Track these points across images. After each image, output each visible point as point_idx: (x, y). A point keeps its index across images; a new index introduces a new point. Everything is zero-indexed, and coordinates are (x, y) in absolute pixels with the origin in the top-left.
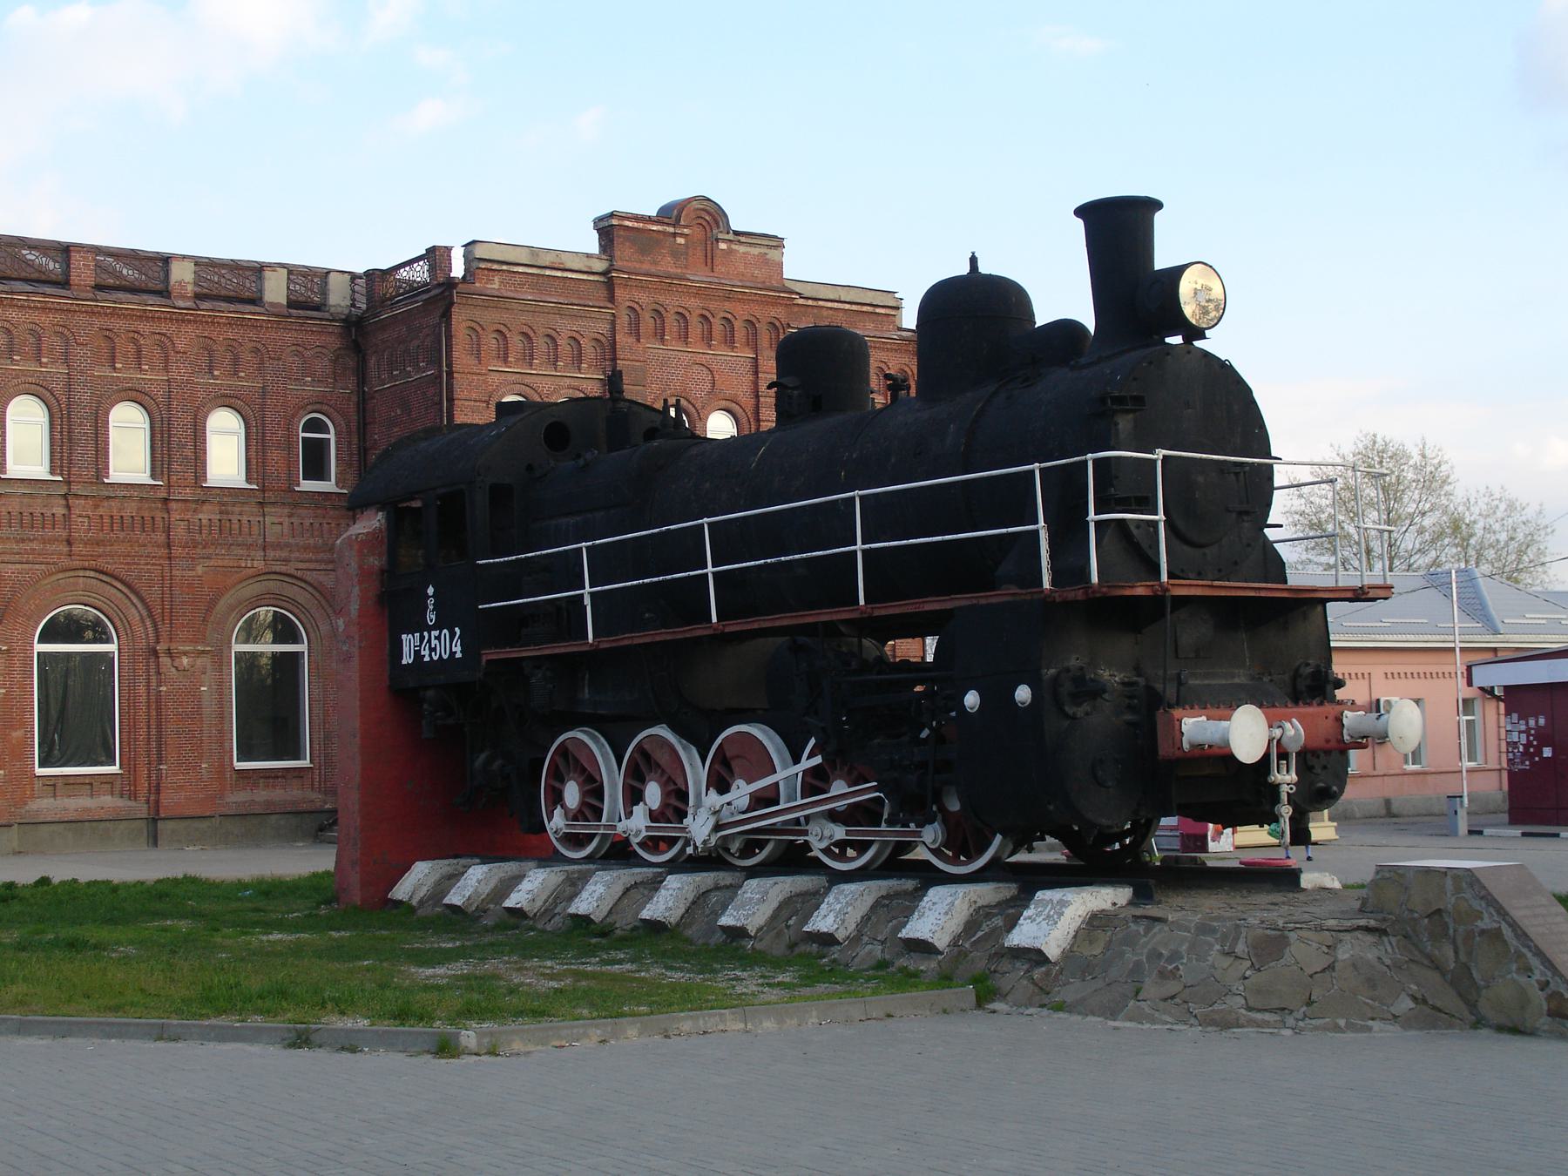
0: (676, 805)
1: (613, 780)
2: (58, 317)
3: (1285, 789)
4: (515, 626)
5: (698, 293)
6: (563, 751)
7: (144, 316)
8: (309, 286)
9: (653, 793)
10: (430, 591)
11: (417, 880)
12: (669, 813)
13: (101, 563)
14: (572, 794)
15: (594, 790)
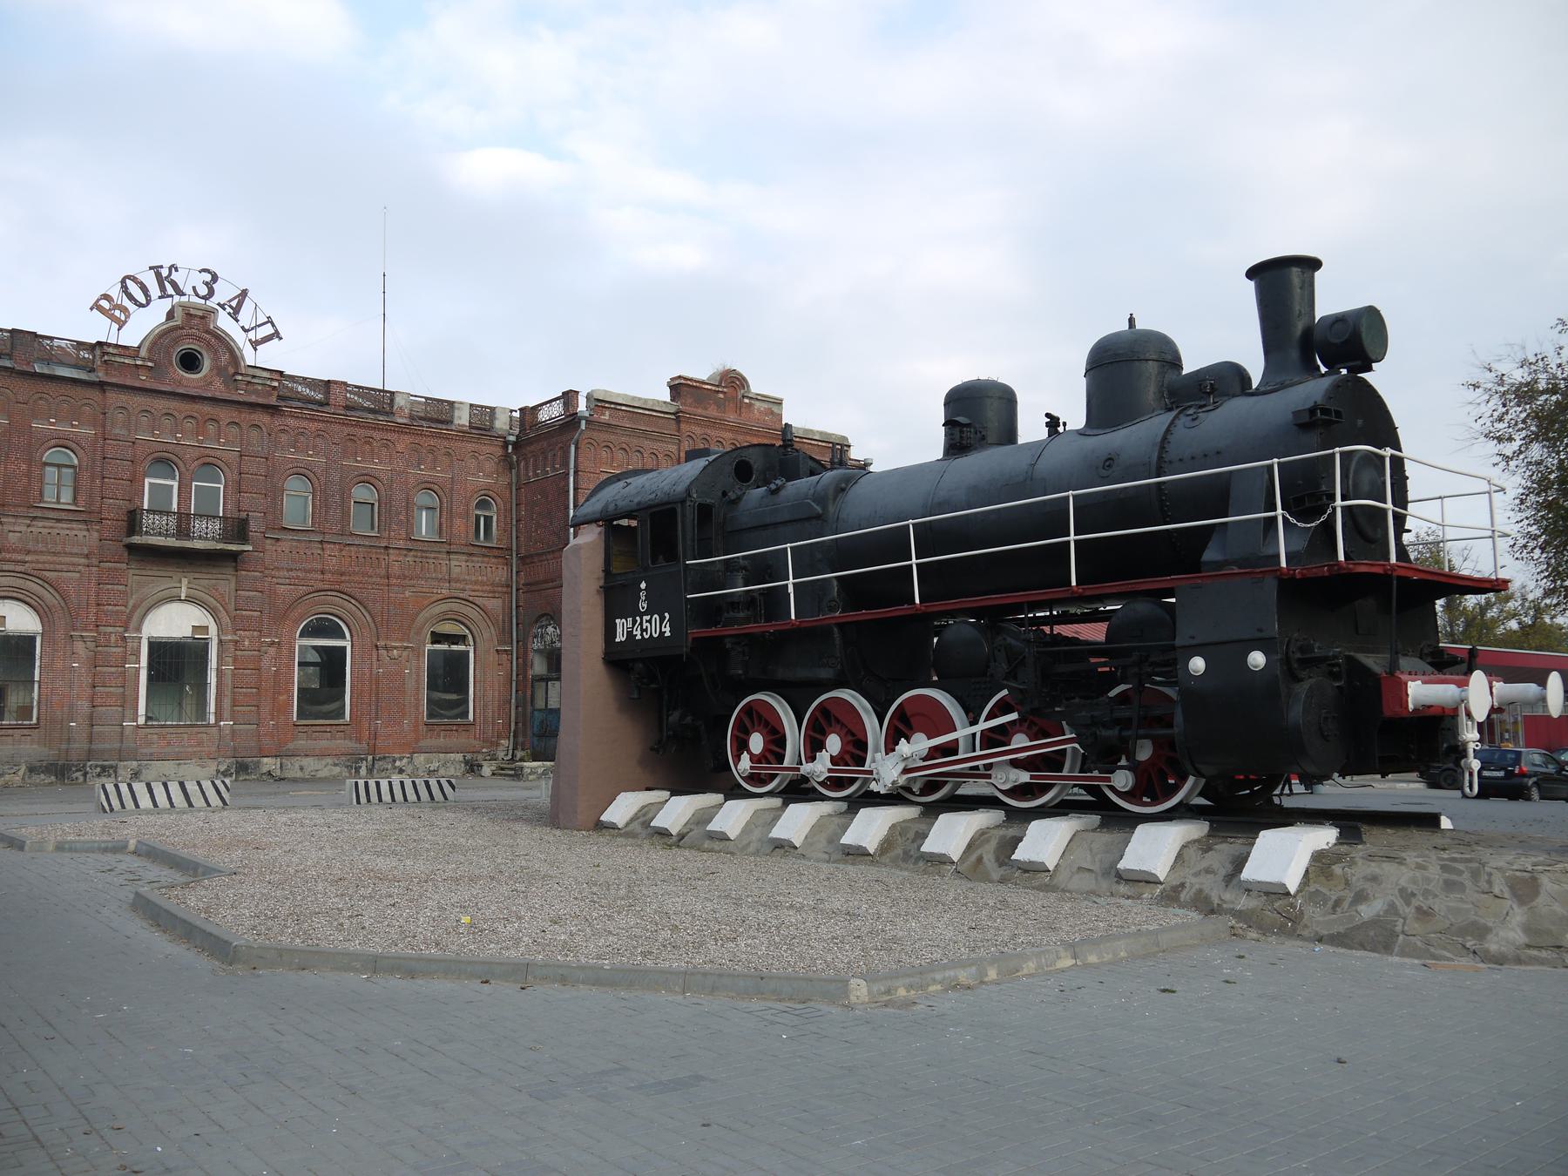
0: (856, 750)
1: (794, 738)
2: (321, 425)
3: (1471, 746)
4: (711, 611)
5: (732, 429)
6: (748, 709)
7: (376, 428)
8: (484, 416)
9: (834, 743)
10: (643, 585)
11: (623, 808)
12: (847, 757)
13: (343, 587)
14: (757, 742)
15: (776, 740)
